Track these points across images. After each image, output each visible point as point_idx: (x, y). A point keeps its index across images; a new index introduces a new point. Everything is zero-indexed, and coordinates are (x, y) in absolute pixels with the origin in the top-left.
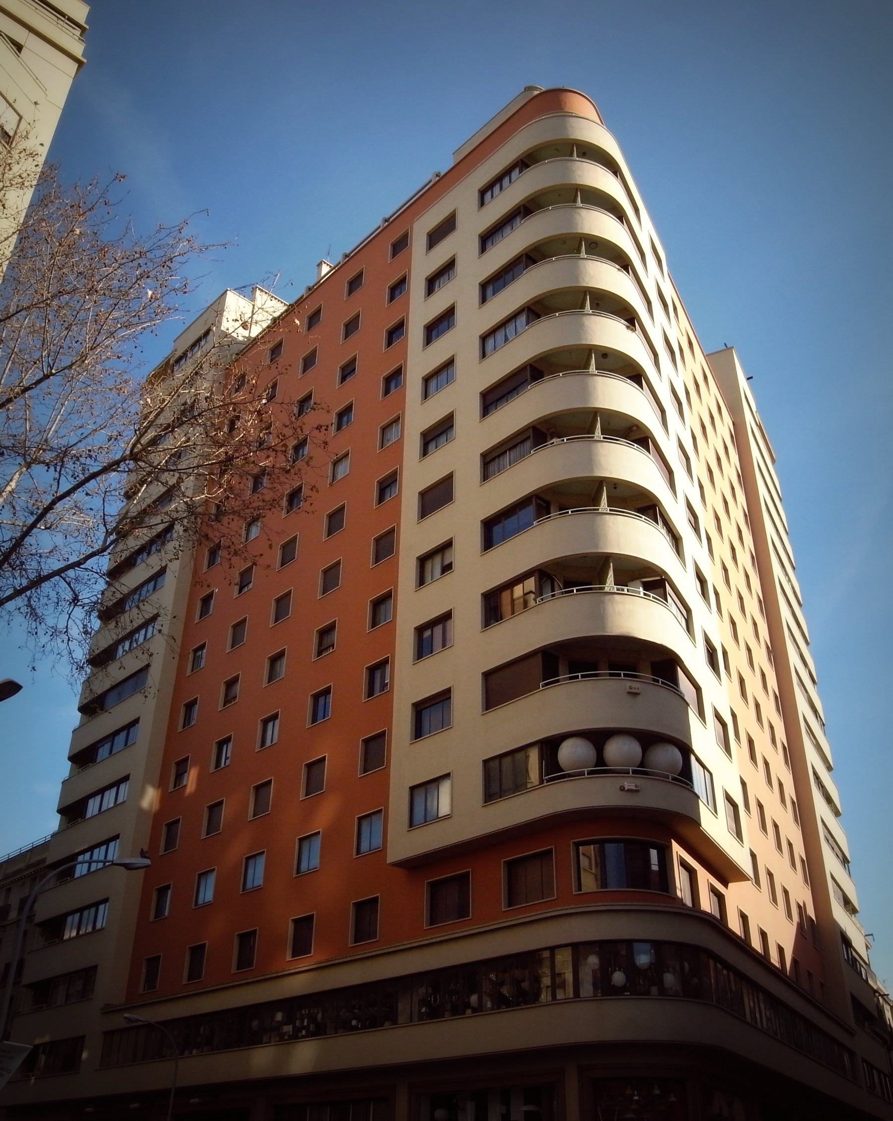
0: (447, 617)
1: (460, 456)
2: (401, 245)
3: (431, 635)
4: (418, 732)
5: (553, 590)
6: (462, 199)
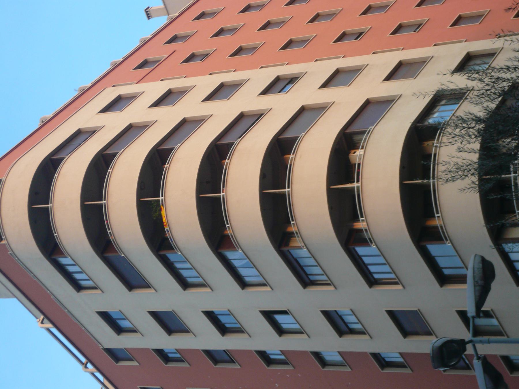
0: (392, 314)
1: (188, 306)
2: (115, 355)
3: (168, 322)
4: (184, 330)
5: (361, 231)
6: (83, 307)
